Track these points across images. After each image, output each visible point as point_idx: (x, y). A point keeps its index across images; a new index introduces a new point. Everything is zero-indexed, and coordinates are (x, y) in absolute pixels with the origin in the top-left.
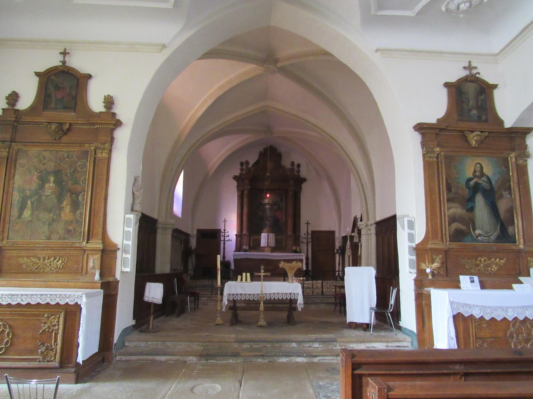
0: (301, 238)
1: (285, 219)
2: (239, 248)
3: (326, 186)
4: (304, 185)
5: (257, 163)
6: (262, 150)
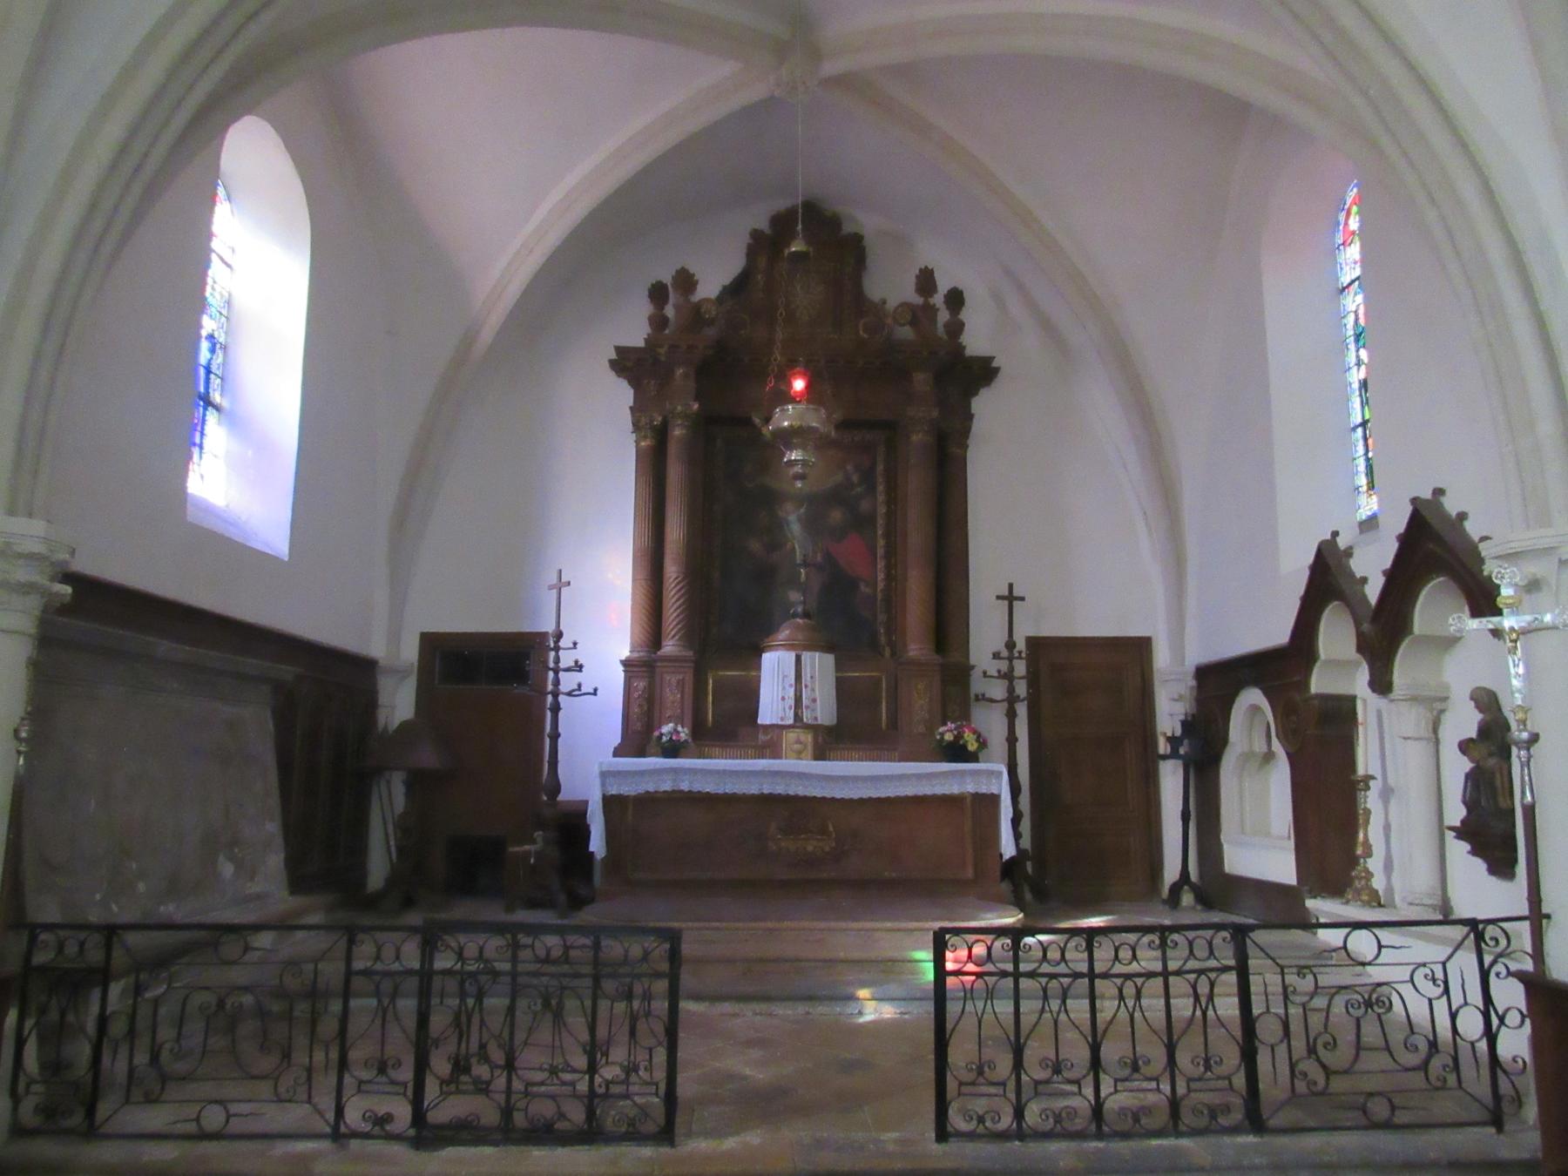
0: (976, 675)
1: (889, 577)
2: (637, 739)
3: (1102, 411)
4: (984, 405)
5: (738, 288)
6: (763, 224)
